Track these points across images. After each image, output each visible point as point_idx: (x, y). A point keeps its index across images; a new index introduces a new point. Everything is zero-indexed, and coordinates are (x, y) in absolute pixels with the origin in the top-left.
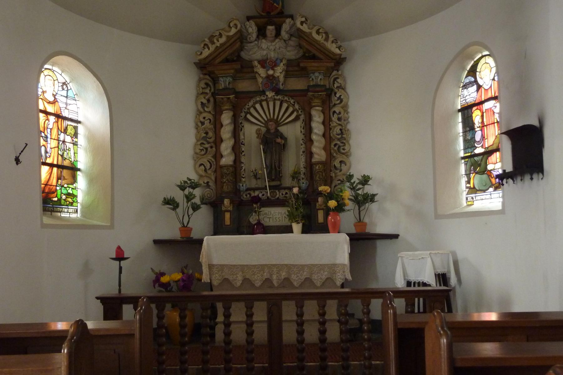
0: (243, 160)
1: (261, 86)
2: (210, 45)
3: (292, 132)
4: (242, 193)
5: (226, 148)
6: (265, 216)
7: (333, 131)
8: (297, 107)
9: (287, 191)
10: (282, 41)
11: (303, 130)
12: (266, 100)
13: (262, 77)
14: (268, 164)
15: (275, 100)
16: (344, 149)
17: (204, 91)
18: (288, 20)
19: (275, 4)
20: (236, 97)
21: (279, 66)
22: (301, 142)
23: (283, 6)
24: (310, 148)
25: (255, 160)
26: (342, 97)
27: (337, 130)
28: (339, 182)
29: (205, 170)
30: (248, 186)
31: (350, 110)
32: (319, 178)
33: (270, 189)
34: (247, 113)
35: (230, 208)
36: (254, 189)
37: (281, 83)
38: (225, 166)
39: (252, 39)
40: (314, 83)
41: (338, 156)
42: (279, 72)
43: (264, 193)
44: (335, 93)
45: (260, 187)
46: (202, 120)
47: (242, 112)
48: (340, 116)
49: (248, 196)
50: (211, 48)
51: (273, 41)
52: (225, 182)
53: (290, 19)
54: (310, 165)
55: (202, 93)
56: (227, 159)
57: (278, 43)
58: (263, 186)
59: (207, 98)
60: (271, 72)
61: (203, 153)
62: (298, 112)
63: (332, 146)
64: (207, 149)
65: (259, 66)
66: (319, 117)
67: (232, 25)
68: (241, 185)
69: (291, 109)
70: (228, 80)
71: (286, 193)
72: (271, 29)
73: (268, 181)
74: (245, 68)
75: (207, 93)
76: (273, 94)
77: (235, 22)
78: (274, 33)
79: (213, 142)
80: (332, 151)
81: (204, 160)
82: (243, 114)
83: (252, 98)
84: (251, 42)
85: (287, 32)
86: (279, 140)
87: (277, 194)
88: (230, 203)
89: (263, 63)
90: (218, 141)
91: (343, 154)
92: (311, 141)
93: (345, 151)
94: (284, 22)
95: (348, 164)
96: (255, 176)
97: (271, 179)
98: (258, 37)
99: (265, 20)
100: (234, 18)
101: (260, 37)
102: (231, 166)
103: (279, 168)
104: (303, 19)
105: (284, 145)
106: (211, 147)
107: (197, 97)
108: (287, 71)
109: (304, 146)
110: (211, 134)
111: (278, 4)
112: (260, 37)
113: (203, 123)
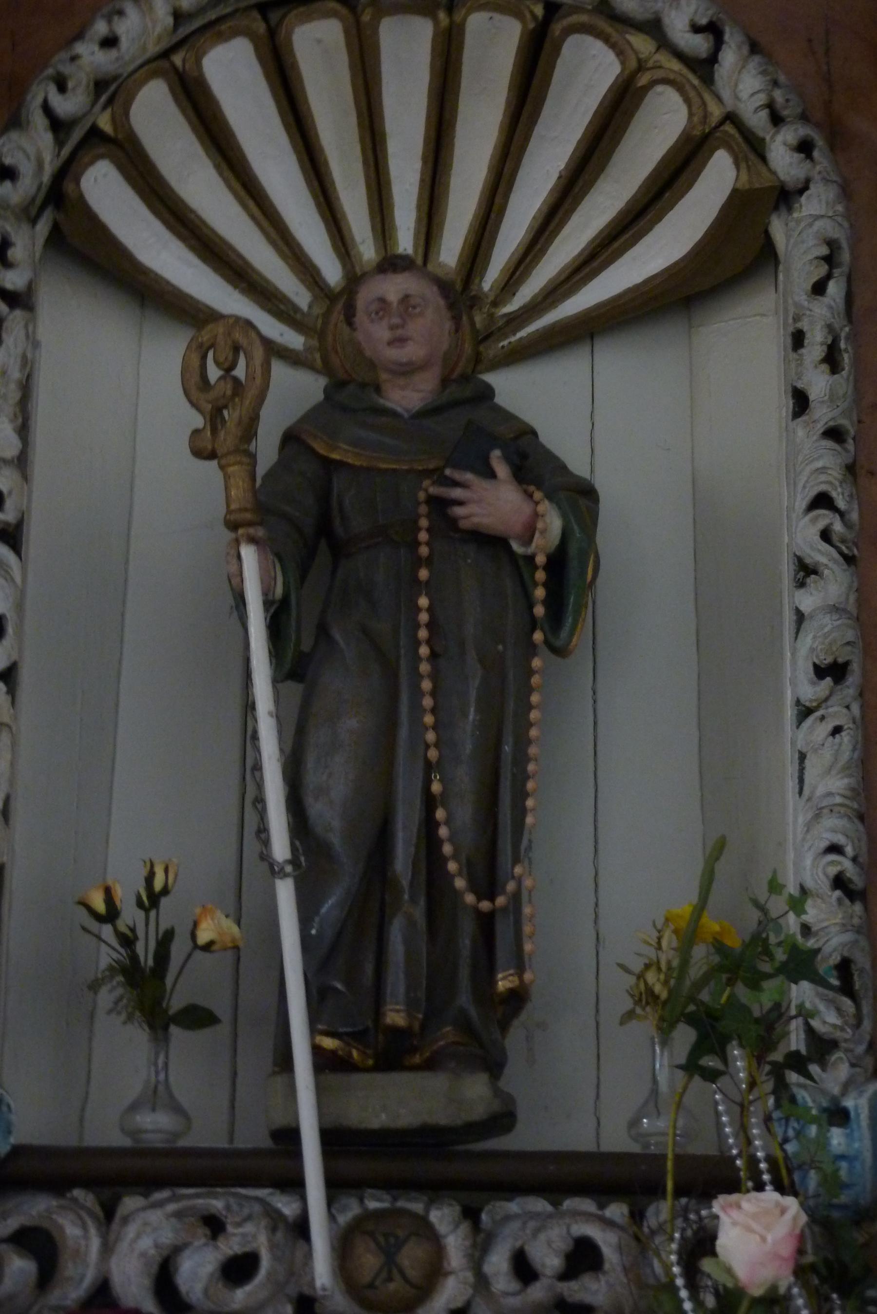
8: (743, 85)
9: (601, 1225)
11: (818, 383)
22: (805, 535)
33: (335, 1185)
43: (247, 1234)
45: (207, 1133)
58: (253, 1136)
62: (752, 148)
69: (663, 123)
71: (583, 1257)
73: (324, 1063)
86: (495, 502)
87: (435, 1271)
96: (146, 986)
97: (361, 1045)
105: (558, 562)
109: (834, 584)
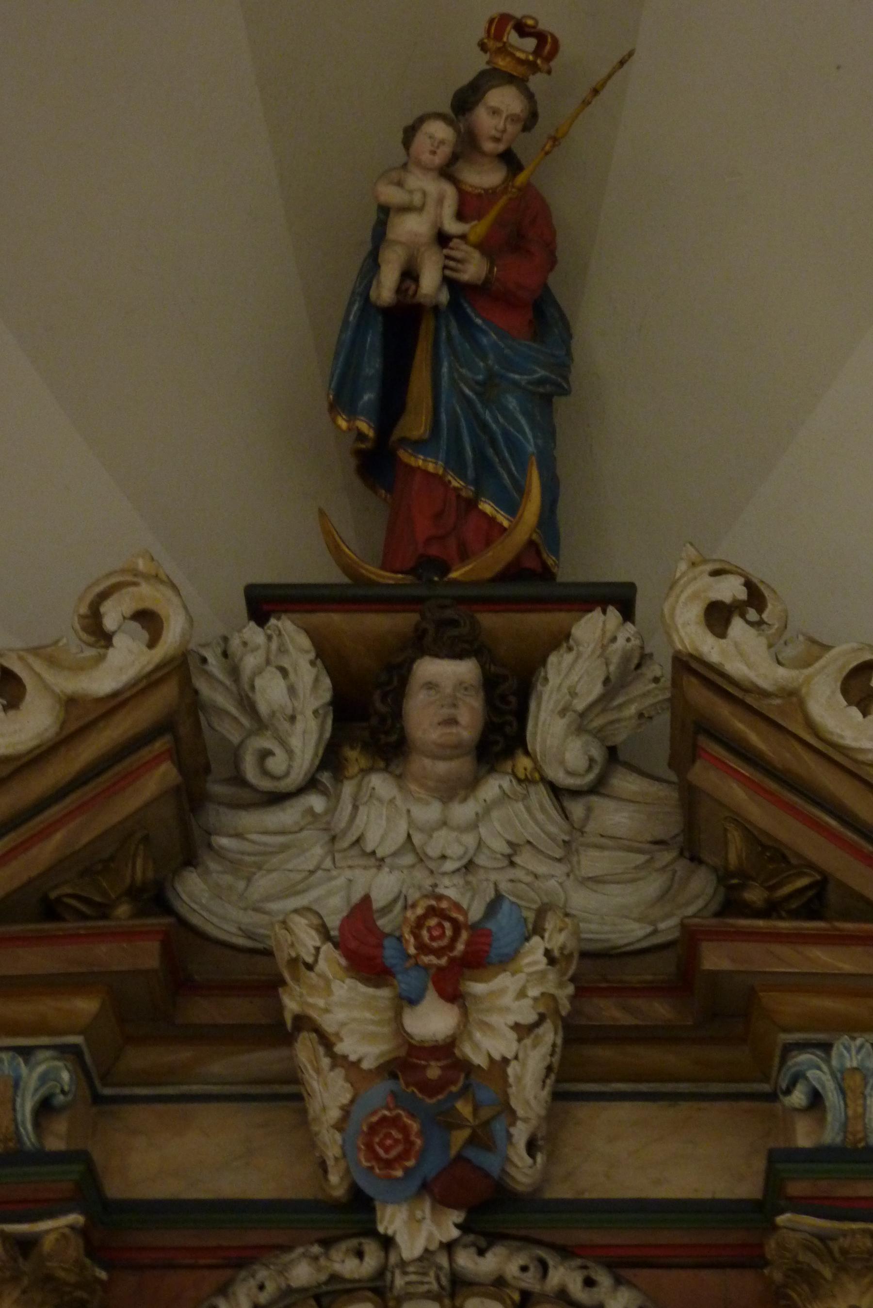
1: (331, 1143)
10: (540, 795)
13: (350, 1067)
18: (592, 627)
19: (487, 507)
20: (94, 1244)
21: (508, 961)
23: (548, 519)
37: (521, 1133)
39: (277, 764)
40: (831, 1136)
42: (506, 1020)
51: (452, 791)
53: (613, 615)
57: (502, 813)
60: (433, 1021)
65: (330, 961)
67: (112, 615)
70: (31, 1076)
72: (443, 689)
76: (448, 1226)
77: (148, 595)
83: (241, 1261)
84: (276, 799)
85: (581, 724)
89: (364, 947)
94: (561, 639)
98: (331, 760)
99: (402, 622)
100: (141, 565)
101: (354, 756)
104: (730, 589)
108: (576, 1034)
111: (513, 508)
112: (354, 756)
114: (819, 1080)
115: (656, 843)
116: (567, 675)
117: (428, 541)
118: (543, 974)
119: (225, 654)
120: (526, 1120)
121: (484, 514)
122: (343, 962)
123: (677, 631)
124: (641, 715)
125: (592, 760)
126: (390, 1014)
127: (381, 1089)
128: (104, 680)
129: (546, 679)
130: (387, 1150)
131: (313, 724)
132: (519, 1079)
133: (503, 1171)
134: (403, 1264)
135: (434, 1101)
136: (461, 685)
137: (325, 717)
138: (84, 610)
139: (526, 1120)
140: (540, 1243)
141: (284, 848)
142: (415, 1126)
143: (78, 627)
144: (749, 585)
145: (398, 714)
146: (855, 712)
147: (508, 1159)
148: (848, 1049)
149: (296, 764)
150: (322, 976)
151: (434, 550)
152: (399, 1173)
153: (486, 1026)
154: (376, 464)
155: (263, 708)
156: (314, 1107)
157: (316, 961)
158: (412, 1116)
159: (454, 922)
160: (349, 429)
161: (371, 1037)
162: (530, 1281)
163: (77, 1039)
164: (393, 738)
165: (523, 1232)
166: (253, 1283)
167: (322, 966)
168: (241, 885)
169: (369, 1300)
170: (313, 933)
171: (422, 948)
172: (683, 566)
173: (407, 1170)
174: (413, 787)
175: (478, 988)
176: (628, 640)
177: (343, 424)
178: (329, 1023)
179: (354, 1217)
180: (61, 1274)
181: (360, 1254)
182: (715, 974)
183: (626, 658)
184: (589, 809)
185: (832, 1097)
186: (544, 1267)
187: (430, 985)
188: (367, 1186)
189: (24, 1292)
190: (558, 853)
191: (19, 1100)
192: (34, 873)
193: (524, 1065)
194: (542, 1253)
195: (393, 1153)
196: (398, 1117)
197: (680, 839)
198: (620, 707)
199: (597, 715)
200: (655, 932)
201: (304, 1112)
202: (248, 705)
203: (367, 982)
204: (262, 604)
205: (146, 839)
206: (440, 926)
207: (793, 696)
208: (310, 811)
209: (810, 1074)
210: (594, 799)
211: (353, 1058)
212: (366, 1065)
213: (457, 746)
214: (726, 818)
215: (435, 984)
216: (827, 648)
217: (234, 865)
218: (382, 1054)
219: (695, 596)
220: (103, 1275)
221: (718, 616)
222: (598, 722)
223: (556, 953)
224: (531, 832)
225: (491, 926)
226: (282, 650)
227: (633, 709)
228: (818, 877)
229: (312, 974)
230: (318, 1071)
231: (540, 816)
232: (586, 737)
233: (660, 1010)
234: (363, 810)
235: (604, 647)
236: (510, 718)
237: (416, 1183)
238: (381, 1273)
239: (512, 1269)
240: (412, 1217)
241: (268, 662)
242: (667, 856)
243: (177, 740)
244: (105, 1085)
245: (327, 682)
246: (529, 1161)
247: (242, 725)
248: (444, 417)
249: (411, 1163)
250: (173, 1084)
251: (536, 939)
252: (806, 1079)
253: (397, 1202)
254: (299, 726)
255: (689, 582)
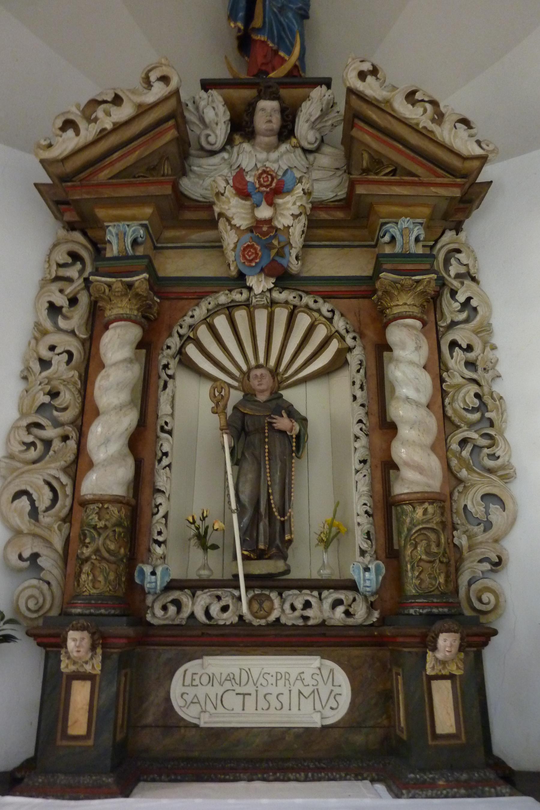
0: (161, 482)
2: (82, 125)
3: (327, 406)
4: (149, 599)
5: (108, 437)
6: (228, 685)
7: (453, 400)
8: (340, 324)
10: (299, 151)
12: (247, 305)
14: (245, 498)
15: (273, 303)
16: (493, 457)
17: (64, 272)
18: (317, 93)
19: (282, 54)
21: (289, 192)
22: (356, 429)
24: (388, 450)
25: (200, 483)
26: (474, 303)
27: (467, 395)
28: (487, 566)
29: (34, 513)
30: (176, 573)
31: (496, 340)
32: (428, 553)
33: (247, 588)
34: (186, 340)
35: (95, 666)
36: (194, 586)
37: (294, 252)
38: (93, 501)
39: (212, 139)
41: (475, 477)
42: (288, 214)
43: (227, 600)
44: (453, 293)
45: (217, 575)
46: (45, 354)
47: (170, 335)
48: (471, 356)
49: (172, 609)
50: (83, 132)
52: (87, 559)
53: (324, 87)
54: (387, 506)
55: (58, 279)
56: (108, 477)
58: (228, 576)
59: (68, 291)
60: (264, 212)
61: (33, 454)
63: (455, 446)
64: (48, 443)
66: (418, 348)
67: (153, 77)
68: (148, 569)
69: (321, 332)
71: (307, 605)
72: (267, 113)
73: (245, 558)
74: (191, 216)
75: (69, 280)
76: (270, 283)
78: (276, 122)
79: (73, 423)
80: (454, 462)
81: (35, 482)
82: (174, 342)
83: (201, 297)
84: (212, 153)
85: (313, 126)
86: (283, 423)
87: (272, 609)
88: (93, 648)
90: (87, 412)
91: (490, 471)
92: (389, 428)
93: (499, 462)
94: (306, 97)
95: (509, 505)
96: (202, 539)
97: (254, 553)
98: (230, 141)
100: (163, 61)
101: (237, 138)
102: (115, 500)
103: (283, 514)
104: (366, 67)
105: (298, 437)
106: (65, 438)
107: (42, 287)
108: (313, 224)
109: (364, 441)
110: (67, 397)
111: (289, 52)
112: (237, 138)
113: (45, 364)
114: (394, 232)
115: (337, 169)
116: (309, 109)
117: (263, 64)
118: (302, 197)
119: (194, 102)
120: (295, 248)
121: (280, 56)
122: (234, 192)
123: (348, 80)
124: (332, 125)
125: (316, 139)
126: (250, 211)
127: (248, 235)
128: (151, 97)
129: (301, 111)
130: (249, 256)
131: (224, 127)
132: (293, 234)
133: (288, 266)
134: (255, 295)
135: (265, 238)
136: (273, 110)
137: (228, 124)
138: (143, 76)
139: (295, 248)
140: (299, 290)
141: (215, 170)
142: (259, 248)
143: (142, 82)
144: (373, 65)
145: (252, 122)
146: (410, 106)
147: (289, 261)
148: (404, 222)
149: (218, 140)
150: (227, 197)
151: (264, 68)
152: (254, 264)
153: (282, 215)
154: (244, 43)
155: (207, 120)
156: (225, 245)
157: (225, 192)
158: (258, 244)
159: (271, 175)
160: (235, 27)
161: (243, 219)
162: (296, 302)
163: (146, 222)
164: (250, 129)
165: (294, 287)
166: (207, 302)
167: (227, 193)
168: (201, 182)
169: (245, 309)
170: (224, 182)
171: (261, 185)
172: (350, 60)
173: (256, 263)
174: (257, 148)
175: (279, 201)
176: (329, 96)
177: (232, 25)
178: (229, 214)
179: (240, 280)
180: (141, 293)
181: (241, 293)
182: (360, 195)
183: (328, 104)
184: (315, 158)
185: (398, 237)
186: (301, 297)
187: (264, 200)
188: (244, 271)
189: (130, 300)
190: (305, 171)
191: (126, 239)
192: (129, 164)
193: (295, 229)
194: (300, 293)
195: (251, 258)
196: (253, 245)
197: (345, 167)
198: (326, 121)
199: (318, 124)
200: (336, 196)
201: (223, 252)
202: (202, 120)
203: (242, 199)
204: (207, 85)
205: (167, 158)
206: (267, 177)
207: (388, 102)
208: (223, 158)
209: (391, 230)
210: (316, 154)
211: (238, 225)
212: (242, 228)
213: (271, 130)
214: (363, 150)
215: (265, 199)
216: (398, 88)
217: (199, 176)
218: (249, 224)
219: (355, 69)
220: (158, 300)
221: (362, 75)
222: (318, 126)
223: (306, 191)
224: (296, 163)
225: (284, 178)
226: (213, 101)
227: (330, 123)
228: (394, 168)
229: (223, 197)
230: (226, 232)
231: (299, 158)
232: (314, 130)
233: (340, 215)
234: (241, 156)
235: (321, 99)
236: (289, 123)
237: (258, 270)
238: (248, 300)
239: (291, 298)
240: (258, 280)
241: (208, 104)
242: (340, 173)
243: (176, 121)
244: (157, 243)
245: (228, 113)
246: (296, 262)
247: (200, 127)
248: (267, 19)
249: (257, 261)
250: (180, 243)
251: (299, 184)
252: (389, 232)
253: (253, 275)
254: (219, 127)
255: (352, 64)
